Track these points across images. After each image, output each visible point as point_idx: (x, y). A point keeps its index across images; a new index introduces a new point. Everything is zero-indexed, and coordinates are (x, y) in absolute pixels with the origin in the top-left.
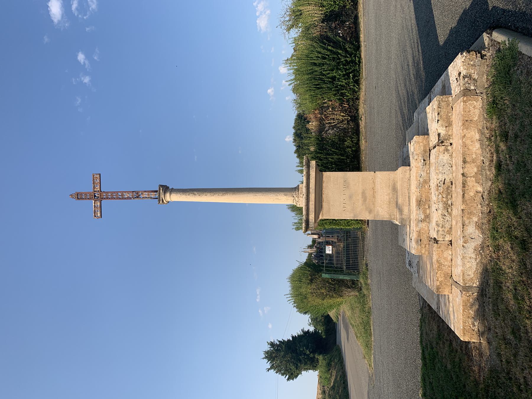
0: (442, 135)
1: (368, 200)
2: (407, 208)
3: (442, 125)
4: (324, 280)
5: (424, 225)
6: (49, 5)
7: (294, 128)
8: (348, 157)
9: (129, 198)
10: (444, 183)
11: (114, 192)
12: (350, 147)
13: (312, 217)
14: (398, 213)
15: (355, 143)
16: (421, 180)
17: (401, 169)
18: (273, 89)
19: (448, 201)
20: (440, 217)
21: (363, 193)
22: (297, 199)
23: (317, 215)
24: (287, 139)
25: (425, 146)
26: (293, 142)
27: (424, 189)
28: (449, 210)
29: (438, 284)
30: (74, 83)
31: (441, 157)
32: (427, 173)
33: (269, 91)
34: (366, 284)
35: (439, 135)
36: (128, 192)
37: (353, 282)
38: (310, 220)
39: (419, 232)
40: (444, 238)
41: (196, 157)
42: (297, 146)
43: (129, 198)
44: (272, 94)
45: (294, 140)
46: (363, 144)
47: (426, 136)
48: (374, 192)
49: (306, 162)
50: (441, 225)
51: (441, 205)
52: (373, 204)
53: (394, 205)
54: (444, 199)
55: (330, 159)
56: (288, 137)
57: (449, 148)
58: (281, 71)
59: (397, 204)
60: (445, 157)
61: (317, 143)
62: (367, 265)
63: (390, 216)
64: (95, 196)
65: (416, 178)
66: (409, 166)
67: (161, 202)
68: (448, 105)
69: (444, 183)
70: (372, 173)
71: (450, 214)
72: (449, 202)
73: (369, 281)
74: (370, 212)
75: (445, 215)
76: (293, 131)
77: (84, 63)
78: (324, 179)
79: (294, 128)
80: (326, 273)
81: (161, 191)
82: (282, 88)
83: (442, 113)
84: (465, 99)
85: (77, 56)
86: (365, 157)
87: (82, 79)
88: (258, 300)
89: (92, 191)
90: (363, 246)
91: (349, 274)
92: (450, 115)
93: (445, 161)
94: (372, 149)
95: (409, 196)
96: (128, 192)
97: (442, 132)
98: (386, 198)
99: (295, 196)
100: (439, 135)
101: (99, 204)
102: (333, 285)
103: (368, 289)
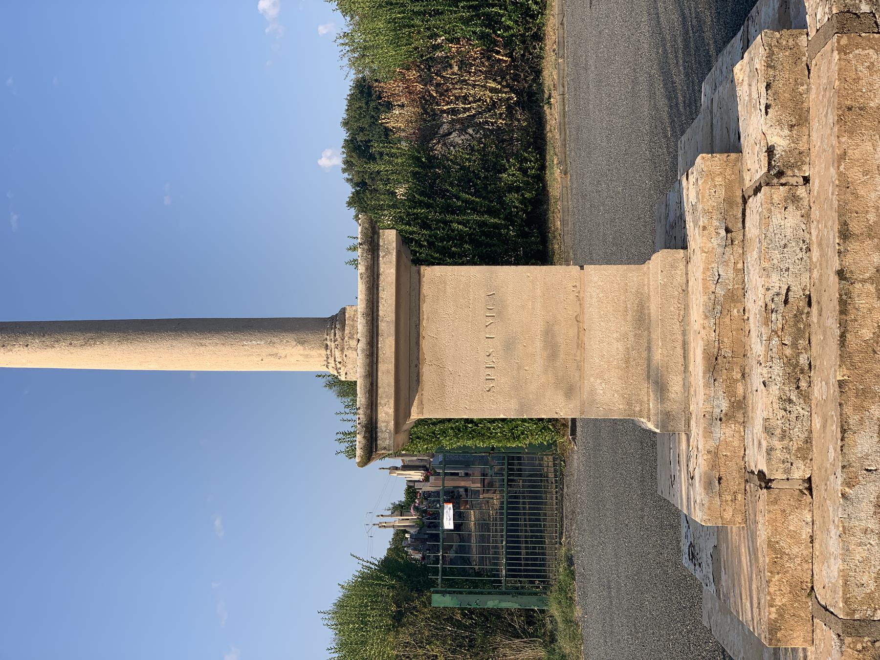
0: (778, 152)
1: (562, 355)
3: (780, 122)
5: (729, 432)
7: (346, 123)
10: (786, 302)
13: (386, 413)
15: (533, 177)
16: (720, 292)
17: (660, 258)
20: (776, 406)
21: (549, 333)
22: (337, 353)
24: (324, 162)
25: (729, 187)
26: (344, 171)
27: (727, 320)
28: (803, 384)
29: (773, 616)
31: (777, 219)
32: (736, 270)
34: (568, 621)
35: (770, 151)
38: (381, 425)
39: (714, 454)
40: (787, 471)
42: (357, 185)
45: (346, 162)
47: (733, 156)
48: (581, 331)
50: (778, 431)
51: (778, 369)
52: (579, 368)
54: (788, 352)
56: (328, 153)
57: (801, 191)
59: (649, 366)
62: (570, 561)
63: (629, 404)
65: (705, 288)
66: (685, 247)
69: (786, 302)
70: (574, 269)
72: (803, 360)
74: (570, 392)
75: (790, 401)
76: (343, 134)
78: (426, 289)
79: (346, 123)
80: (443, 593)
83: (778, 85)
84: (844, 41)
86: (562, 224)
90: (560, 502)
91: (518, 592)
93: (789, 232)
94: (584, 196)
98: (617, 348)
100: (770, 151)
102: (466, 628)
103: (573, 637)
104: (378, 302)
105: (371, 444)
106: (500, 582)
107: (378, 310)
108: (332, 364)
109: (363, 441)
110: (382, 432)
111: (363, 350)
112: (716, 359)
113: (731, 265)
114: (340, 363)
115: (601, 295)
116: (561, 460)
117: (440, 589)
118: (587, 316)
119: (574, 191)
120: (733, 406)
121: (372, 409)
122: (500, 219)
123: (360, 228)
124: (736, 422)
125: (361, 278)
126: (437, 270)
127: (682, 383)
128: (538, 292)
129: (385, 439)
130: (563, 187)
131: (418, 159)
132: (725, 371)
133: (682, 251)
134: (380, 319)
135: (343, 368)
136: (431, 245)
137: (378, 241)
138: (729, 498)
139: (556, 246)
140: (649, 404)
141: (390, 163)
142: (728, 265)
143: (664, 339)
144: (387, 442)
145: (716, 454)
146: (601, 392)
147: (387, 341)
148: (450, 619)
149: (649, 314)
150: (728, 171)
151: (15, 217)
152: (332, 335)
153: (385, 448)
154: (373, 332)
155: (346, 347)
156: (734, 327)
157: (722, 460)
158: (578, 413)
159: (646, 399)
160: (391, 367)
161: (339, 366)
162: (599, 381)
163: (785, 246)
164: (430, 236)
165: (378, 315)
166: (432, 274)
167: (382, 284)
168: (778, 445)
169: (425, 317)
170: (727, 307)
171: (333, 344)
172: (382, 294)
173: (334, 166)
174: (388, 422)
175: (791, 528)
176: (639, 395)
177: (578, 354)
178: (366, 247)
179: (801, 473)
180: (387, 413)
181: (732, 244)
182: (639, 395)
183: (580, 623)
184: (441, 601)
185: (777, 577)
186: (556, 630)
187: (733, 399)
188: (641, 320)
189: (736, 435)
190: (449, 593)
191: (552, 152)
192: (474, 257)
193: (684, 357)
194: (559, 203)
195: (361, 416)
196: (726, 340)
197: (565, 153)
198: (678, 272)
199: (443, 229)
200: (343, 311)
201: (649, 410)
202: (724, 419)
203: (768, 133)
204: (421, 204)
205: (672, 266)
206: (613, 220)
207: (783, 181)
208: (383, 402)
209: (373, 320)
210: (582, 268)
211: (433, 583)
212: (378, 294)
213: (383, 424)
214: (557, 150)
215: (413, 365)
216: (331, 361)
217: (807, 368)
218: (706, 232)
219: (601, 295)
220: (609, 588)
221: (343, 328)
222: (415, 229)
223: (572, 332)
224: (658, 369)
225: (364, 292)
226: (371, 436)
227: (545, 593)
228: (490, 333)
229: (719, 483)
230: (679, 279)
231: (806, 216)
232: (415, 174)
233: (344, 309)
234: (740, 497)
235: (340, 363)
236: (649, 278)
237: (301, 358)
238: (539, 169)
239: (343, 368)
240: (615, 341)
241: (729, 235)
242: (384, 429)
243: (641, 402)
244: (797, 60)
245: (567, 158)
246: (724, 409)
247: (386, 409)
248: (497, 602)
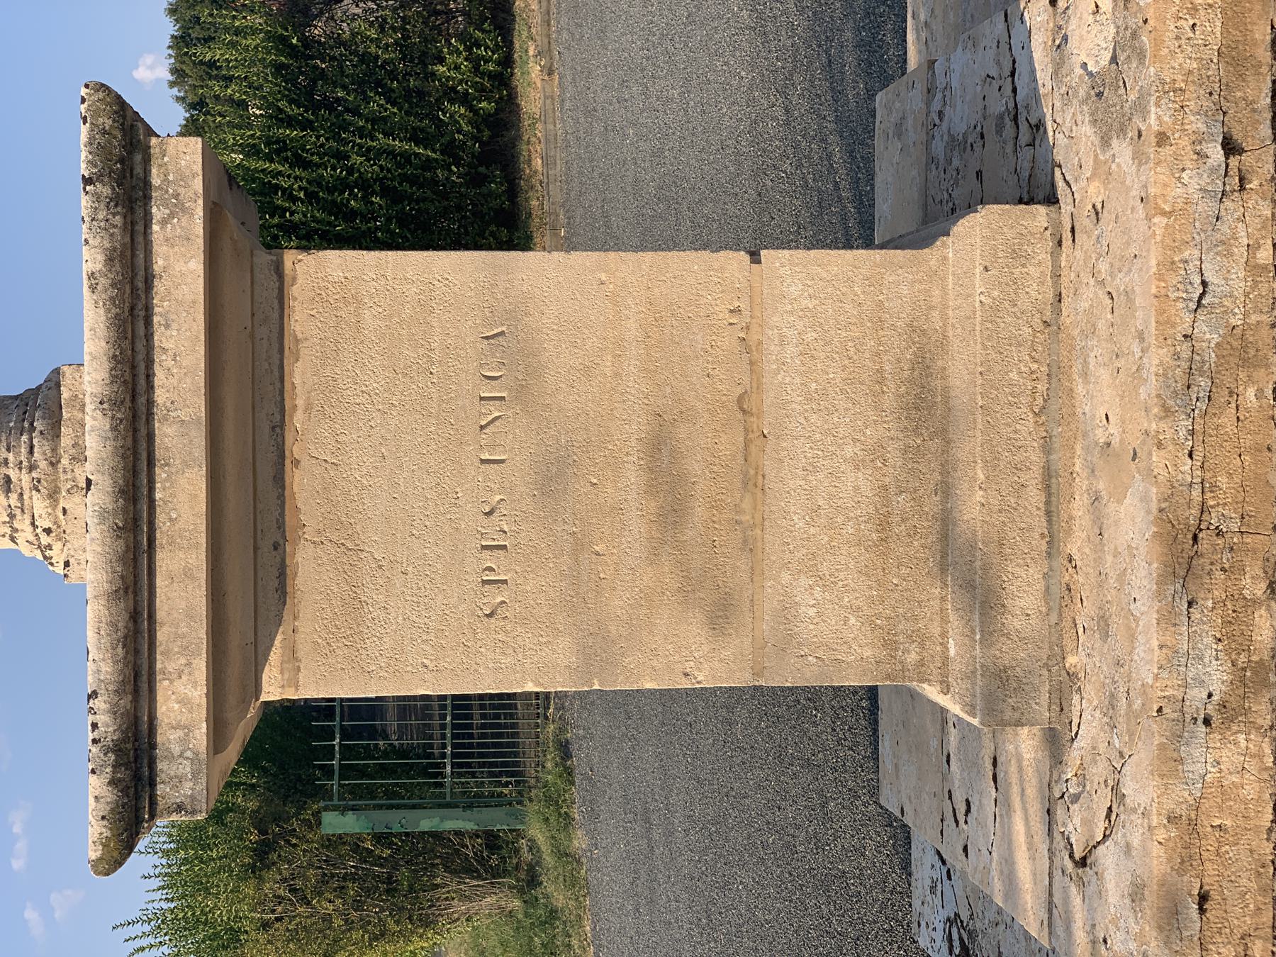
1: (699, 511)
2: (1035, 573)
4: (333, 842)
5: (1230, 757)
7: (172, 11)
12: (465, 100)
13: (182, 700)
14: (955, 623)
15: (491, 76)
16: (1209, 335)
17: (979, 232)
21: (660, 448)
22: (39, 505)
24: (142, 74)
26: (172, 84)
27: (1227, 420)
34: (563, 854)
37: (492, 840)
38: (167, 737)
39: (1187, 824)
42: (193, 106)
45: (174, 71)
46: (534, 86)
48: (754, 440)
52: (749, 547)
55: (357, 159)
56: (149, 59)
59: (945, 537)
61: (278, 68)
62: (565, 750)
63: (890, 645)
65: (1164, 323)
66: (1051, 200)
73: (579, 841)
74: (721, 614)
76: (170, 28)
78: (300, 320)
80: (343, 810)
86: (546, 164)
88: (17, 864)
91: (471, 802)
94: (590, 112)
98: (856, 485)
99: (23, 479)
102: (379, 861)
103: (572, 882)
104: (150, 362)
105: (138, 797)
106: (441, 785)
107: (150, 387)
108: (26, 533)
109: (110, 795)
110: (171, 758)
111: (103, 514)
112: (1195, 538)
113: (1240, 252)
114: (48, 531)
115: (811, 335)
117: (336, 802)
118: (769, 398)
119: (568, 105)
120: (1242, 680)
121: (136, 692)
122: (434, 151)
123: (84, 130)
125: (93, 289)
127: (1041, 586)
128: (632, 328)
129: (180, 779)
130: (546, 98)
131: (284, 40)
132: (1219, 575)
133: (1041, 210)
134: (158, 412)
135: (57, 546)
136: (311, 197)
137: (147, 172)
139: (534, 203)
140: (945, 646)
141: (233, 44)
142: (1230, 254)
143: (991, 464)
144: (187, 788)
145: (1193, 824)
146: (812, 612)
147: (182, 481)
148: (356, 848)
149: (946, 389)
152: (24, 450)
153: (180, 808)
154: (135, 454)
155: (64, 487)
156: (1247, 440)
157: (1210, 842)
158: (748, 676)
159: (936, 630)
161: (45, 540)
162: (804, 581)
164: (309, 182)
165: (150, 403)
166: (319, 274)
167: (161, 306)
169: (300, 402)
170: (1228, 380)
171: (26, 478)
172: (163, 338)
173: (158, 80)
174: (188, 728)
176: (915, 619)
177: (747, 505)
178: (105, 190)
180: (184, 701)
181: (1242, 188)
182: (915, 619)
183: (584, 860)
184: (336, 823)
186: (538, 863)
187: (1243, 658)
188: (925, 408)
190: (353, 809)
191: (525, 34)
192: (389, 220)
193: (1048, 513)
194: (539, 126)
195: (102, 719)
196: (1223, 481)
197: (549, 36)
198: (1031, 269)
199: (334, 169)
200: (54, 380)
201: (946, 660)
202: (1216, 721)
204: (290, 122)
205: (1015, 254)
206: (656, 154)
208: (171, 666)
209: (135, 417)
210: (755, 257)
211: (325, 793)
212: (149, 336)
213: (175, 735)
214: (533, 30)
215: (266, 546)
216: (23, 523)
218: (1167, 151)
219: (811, 335)
220: (647, 821)
222: (281, 168)
223: (730, 443)
224: (973, 547)
225: (102, 330)
226: (137, 777)
227: (520, 803)
228: (492, 448)
229: (1202, 910)
230: (1036, 291)
232: (278, 68)
233: (57, 372)
235: (48, 531)
236: (944, 288)
238: (499, 63)
239: (57, 546)
240: (847, 468)
241: (1234, 162)
242: (176, 749)
243: (921, 639)
245: (553, 46)
246: (1217, 688)
247: (183, 687)
248: (436, 821)
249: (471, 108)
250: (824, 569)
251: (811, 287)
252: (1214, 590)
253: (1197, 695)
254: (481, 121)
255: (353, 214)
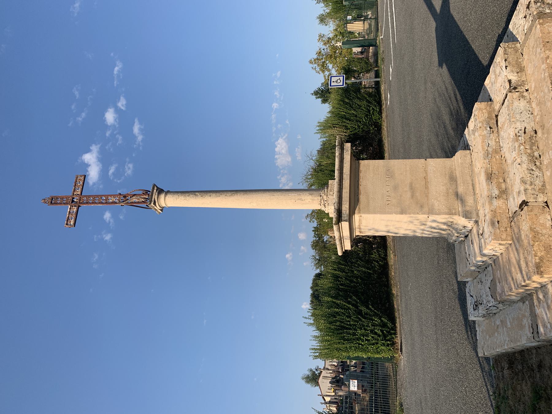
0: (513, 81)
2: (472, 198)
3: (512, 71)
6: (89, 170)
7: (311, 288)
8: (374, 271)
9: (114, 203)
10: (525, 133)
11: (98, 196)
12: (377, 262)
14: (460, 205)
16: (490, 150)
17: (460, 154)
18: (291, 254)
19: (533, 152)
20: (526, 172)
22: (325, 197)
23: (352, 209)
24: (303, 306)
25: (490, 113)
28: (538, 164)
29: (538, 261)
30: (95, 240)
31: (516, 103)
32: (496, 142)
33: (287, 256)
35: (510, 81)
36: (114, 196)
38: (343, 212)
40: (535, 198)
41: (205, 321)
43: (114, 203)
44: (290, 258)
47: (490, 103)
49: (339, 143)
50: (529, 182)
51: (525, 158)
53: (453, 197)
54: (529, 151)
56: (305, 303)
57: (525, 94)
58: (300, 237)
60: (522, 104)
62: (401, 405)
64: (73, 201)
65: (483, 149)
67: (152, 203)
68: (516, 51)
69: (525, 133)
70: (423, 160)
71: (540, 169)
72: (536, 154)
75: (533, 170)
76: (311, 292)
77: (110, 222)
79: (311, 288)
81: (155, 191)
82: (300, 254)
83: (510, 59)
84: (541, 21)
85: (103, 215)
86: (395, 273)
87: (104, 236)
89: (71, 194)
90: (396, 383)
92: (520, 60)
93: (522, 108)
95: (473, 185)
96: (114, 196)
97: (514, 78)
100: (510, 81)
101: (75, 209)
116: (396, 366)
124: (503, 199)
126: (366, 162)
128: (408, 169)
138: (503, 230)
143: (464, 183)
150: (488, 108)
151: (205, 321)
156: (498, 162)
160: (348, 191)
163: (521, 113)
168: (530, 188)
175: (541, 222)
179: (542, 199)
185: (537, 243)
188: (453, 179)
189: (504, 204)
203: (508, 75)
207: (517, 90)
216: (322, 201)
217: (538, 157)
221: (328, 188)
223: (423, 183)
231: (529, 102)
234: (508, 229)
237: (311, 201)
243: (455, 209)
244: (516, 51)
249: (378, 263)
250: (439, 199)
251: (436, 165)
252: (495, 181)
253: (494, 195)
254: (380, 266)
255: (354, 282)
